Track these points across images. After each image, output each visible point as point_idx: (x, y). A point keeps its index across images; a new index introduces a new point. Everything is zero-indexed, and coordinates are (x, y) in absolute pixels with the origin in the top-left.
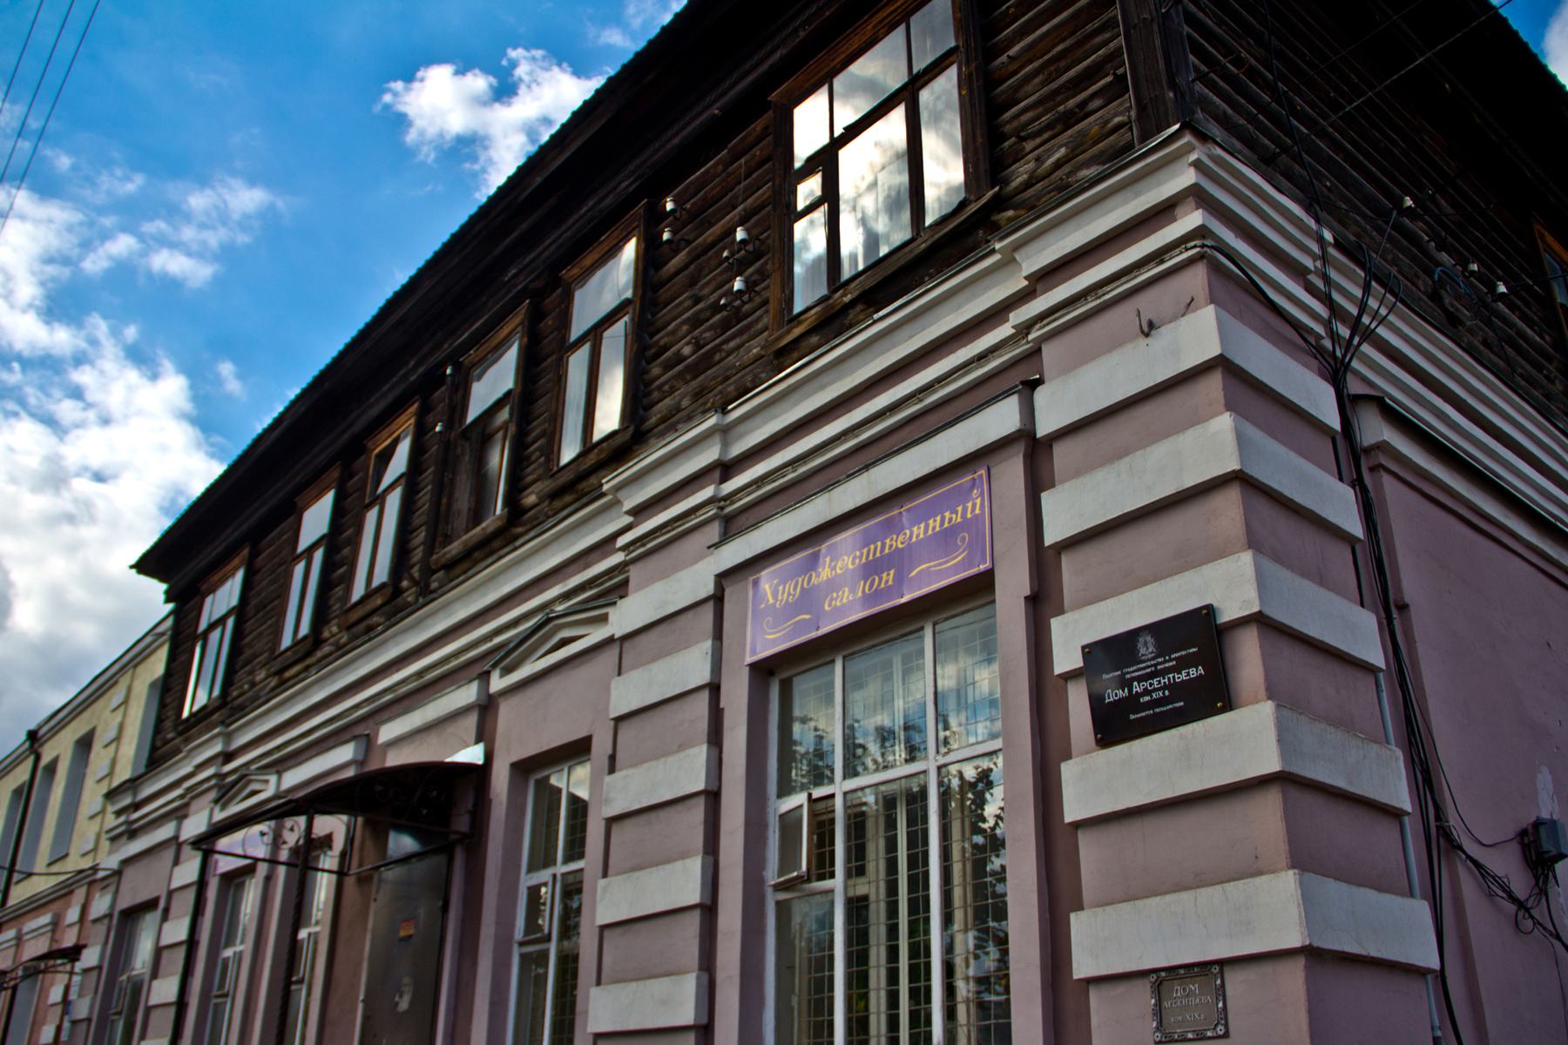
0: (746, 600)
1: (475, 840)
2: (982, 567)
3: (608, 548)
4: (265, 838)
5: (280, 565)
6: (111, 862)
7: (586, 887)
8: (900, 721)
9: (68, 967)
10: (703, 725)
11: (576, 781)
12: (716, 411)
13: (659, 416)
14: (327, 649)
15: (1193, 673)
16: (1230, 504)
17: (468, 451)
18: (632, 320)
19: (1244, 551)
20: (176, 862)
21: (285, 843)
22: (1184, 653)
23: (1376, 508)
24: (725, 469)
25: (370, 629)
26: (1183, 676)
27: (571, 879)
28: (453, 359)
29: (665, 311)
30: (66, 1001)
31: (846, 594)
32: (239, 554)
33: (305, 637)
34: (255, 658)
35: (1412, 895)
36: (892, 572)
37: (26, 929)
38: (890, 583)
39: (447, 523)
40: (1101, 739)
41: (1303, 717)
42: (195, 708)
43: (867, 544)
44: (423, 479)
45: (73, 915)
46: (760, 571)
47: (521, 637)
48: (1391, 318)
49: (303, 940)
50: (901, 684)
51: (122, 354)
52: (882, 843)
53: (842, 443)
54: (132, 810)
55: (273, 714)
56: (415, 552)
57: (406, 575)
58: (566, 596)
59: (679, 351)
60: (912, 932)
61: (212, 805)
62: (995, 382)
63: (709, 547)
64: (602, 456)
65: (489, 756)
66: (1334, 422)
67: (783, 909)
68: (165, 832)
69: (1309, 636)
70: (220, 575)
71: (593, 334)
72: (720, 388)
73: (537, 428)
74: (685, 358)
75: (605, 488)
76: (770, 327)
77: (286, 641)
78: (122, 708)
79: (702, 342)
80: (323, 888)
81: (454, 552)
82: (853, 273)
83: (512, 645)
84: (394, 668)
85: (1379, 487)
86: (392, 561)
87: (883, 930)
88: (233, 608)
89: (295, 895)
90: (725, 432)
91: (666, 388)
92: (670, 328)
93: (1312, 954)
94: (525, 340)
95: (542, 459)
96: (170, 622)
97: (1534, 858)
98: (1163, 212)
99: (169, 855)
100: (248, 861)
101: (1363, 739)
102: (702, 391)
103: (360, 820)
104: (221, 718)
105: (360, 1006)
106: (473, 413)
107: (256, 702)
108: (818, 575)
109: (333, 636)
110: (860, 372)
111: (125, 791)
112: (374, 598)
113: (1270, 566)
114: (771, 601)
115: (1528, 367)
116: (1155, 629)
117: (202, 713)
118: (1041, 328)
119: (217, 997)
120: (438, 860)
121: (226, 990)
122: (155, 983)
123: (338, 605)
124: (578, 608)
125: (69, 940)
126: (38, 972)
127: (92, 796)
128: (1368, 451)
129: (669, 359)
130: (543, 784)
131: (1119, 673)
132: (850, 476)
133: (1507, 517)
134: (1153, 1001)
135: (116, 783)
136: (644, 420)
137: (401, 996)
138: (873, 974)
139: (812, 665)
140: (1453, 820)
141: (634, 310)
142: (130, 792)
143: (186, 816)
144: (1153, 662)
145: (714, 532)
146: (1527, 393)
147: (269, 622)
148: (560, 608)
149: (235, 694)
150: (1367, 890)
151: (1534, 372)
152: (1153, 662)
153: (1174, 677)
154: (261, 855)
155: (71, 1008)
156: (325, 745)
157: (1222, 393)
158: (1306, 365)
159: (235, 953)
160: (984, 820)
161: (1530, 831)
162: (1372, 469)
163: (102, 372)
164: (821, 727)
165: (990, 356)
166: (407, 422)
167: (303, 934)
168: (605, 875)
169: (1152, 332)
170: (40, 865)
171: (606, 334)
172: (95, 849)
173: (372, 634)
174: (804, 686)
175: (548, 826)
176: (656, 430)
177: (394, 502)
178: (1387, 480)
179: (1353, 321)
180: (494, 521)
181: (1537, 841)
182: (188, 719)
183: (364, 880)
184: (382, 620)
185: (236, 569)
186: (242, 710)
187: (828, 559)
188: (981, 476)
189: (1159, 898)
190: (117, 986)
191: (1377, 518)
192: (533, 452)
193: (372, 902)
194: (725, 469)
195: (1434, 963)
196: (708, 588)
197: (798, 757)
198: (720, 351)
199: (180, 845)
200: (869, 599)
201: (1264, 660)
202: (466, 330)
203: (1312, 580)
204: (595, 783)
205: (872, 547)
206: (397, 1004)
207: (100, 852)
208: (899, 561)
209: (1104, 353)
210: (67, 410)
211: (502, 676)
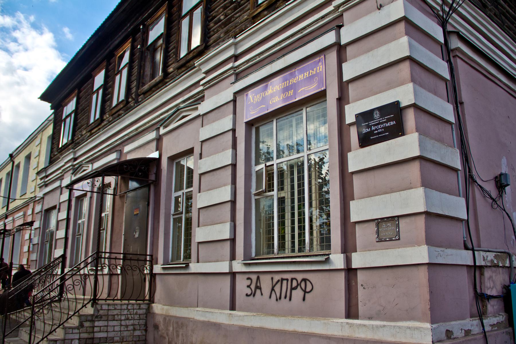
0: (244, 101)
1: (157, 182)
2: (322, 89)
3: (197, 85)
4: (89, 184)
5: (88, 95)
6: (40, 194)
7: (193, 196)
8: (295, 143)
9: (30, 228)
10: (230, 143)
11: (189, 163)
12: (233, 38)
13: (213, 40)
14: (105, 123)
15: (392, 123)
16: (406, 67)
17: (149, 54)
18: (203, 7)
19: (410, 83)
20: (61, 194)
21: (96, 186)
22: (389, 117)
23: (454, 69)
24: (236, 57)
25: (119, 115)
26: (389, 124)
27: (188, 194)
28: (143, 23)
29: (214, 4)
30: (30, 239)
31: (277, 98)
32: (74, 93)
33: (98, 119)
34: (82, 127)
35: (460, 196)
36: (292, 91)
37: (15, 217)
38: (292, 94)
39: (143, 79)
40: (361, 145)
41: (427, 138)
42: (63, 144)
43: (284, 82)
44: (134, 71)
45: (30, 212)
46: (248, 91)
47: (170, 116)
48: (463, 4)
49: (103, 216)
50: (295, 131)
51: (30, 26)
52: (289, 180)
53: (275, 48)
54: (45, 178)
55: (89, 144)
56: (133, 89)
57: (130, 97)
58: (184, 101)
59: (219, 17)
60: (299, 208)
61: (71, 175)
62: (327, 26)
63: (231, 84)
64: (195, 54)
65: (160, 155)
66: (442, 40)
67: (257, 202)
68: (57, 184)
69: (430, 112)
70: (68, 99)
71: (190, 13)
72: (234, 30)
73: (172, 46)
74: (222, 20)
75: (196, 65)
76: (250, 9)
77: (92, 121)
78: (40, 145)
79: (227, 14)
80: (109, 200)
81: (146, 89)
83: (166, 118)
84: (128, 128)
85: (456, 62)
86: (125, 92)
87: (290, 207)
88: (74, 110)
89: (100, 202)
90: (236, 45)
91: (215, 30)
92: (216, 10)
93: (427, 214)
94: (167, 15)
95: (174, 56)
96: (53, 116)
97: (499, 186)
99: (58, 191)
100: (85, 192)
101: (446, 146)
102: (228, 31)
103: (119, 177)
104: (72, 147)
105: (123, 236)
106: (150, 42)
107: (83, 141)
108: (268, 92)
109: (107, 118)
110: (281, 23)
111: (42, 172)
112: (120, 105)
113: (418, 88)
114: (252, 101)
115: (509, 23)
116: (380, 109)
117: (66, 146)
118: (343, 7)
119: (77, 235)
120: (145, 189)
121: (80, 233)
122: (58, 232)
123: (108, 108)
124: (188, 105)
125: (29, 220)
126: (21, 230)
127: (32, 174)
128: (452, 50)
129: (216, 21)
130: (178, 164)
131: (367, 123)
132: (278, 59)
133: (498, 74)
134: (376, 229)
135: (39, 169)
136: (208, 42)
137: (136, 233)
138: (286, 221)
139: (267, 121)
140: (474, 173)
141: (204, 4)
142: (44, 172)
143: (63, 179)
144: (378, 120)
145: (232, 79)
146: (508, 32)
147: (86, 115)
148: (182, 106)
149: (76, 139)
150: (446, 194)
151: (511, 25)
152: (378, 120)
153: (385, 125)
154: (88, 190)
155: (32, 240)
156: (106, 154)
157: (404, 29)
158: (433, 20)
159: (82, 221)
160: (322, 174)
161: (498, 177)
162: (454, 57)
163: (23, 32)
164: (269, 145)
165: (326, 17)
166: (128, 46)
167: (103, 215)
168: (199, 192)
169: (381, 8)
170: (18, 196)
171: (194, 12)
172: (35, 191)
173: (120, 117)
174: (263, 130)
175: (181, 177)
176: (212, 45)
177: (125, 73)
178: (459, 61)
179: (450, 6)
180: (159, 77)
181: (500, 180)
182: (61, 148)
183: (122, 197)
184: (123, 112)
185: (74, 97)
186: (78, 144)
187: (271, 87)
188: (322, 58)
189: (379, 196)
190: (46, 233)
191: (455, 73)
192: (171, 54)
193: (125, 204)
194: (236, 57)
195: (466, 218)
196: (231, 98)
197: (262, 154)
198: (234, 17)
199: (62, 188)
200: (284, 100)
201: (415, 119)
202: (147, 13)
203: (433, 93)
204: (195, 163)
205: (286, 82)
206: (135, 235)
207: (36, 191)
208: (293, 87)
209: (364, 16)
210: (12, 46)
211: (163, 129)
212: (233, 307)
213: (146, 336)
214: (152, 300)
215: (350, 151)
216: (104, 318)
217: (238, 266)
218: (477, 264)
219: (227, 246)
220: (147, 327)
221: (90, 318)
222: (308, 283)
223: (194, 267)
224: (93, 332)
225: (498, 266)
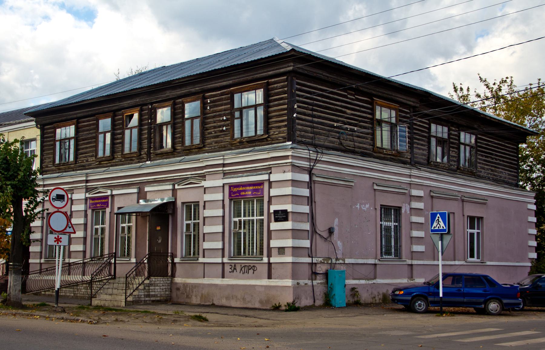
10: (221, 206)
82: (246, 105)
87: (248, 250)
98: (286, 157)
212: (223, 277)
213: (171, 294)
214: (173, 276)
215: (271, 222)
216: (154, 285)
217: (226, 260)
218: (313, 262)
219: (221, 251)
220: (171, 290)
221: (148, 285)
222: (255, 267)
223: (201, 260)
224: (149, 292)
225: (324, 263)
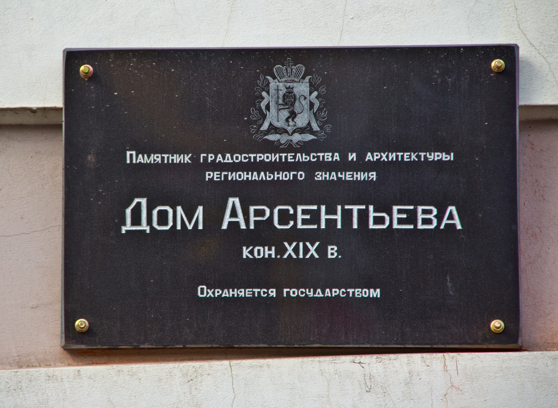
144: (302, 157)
152: (302, 157)
